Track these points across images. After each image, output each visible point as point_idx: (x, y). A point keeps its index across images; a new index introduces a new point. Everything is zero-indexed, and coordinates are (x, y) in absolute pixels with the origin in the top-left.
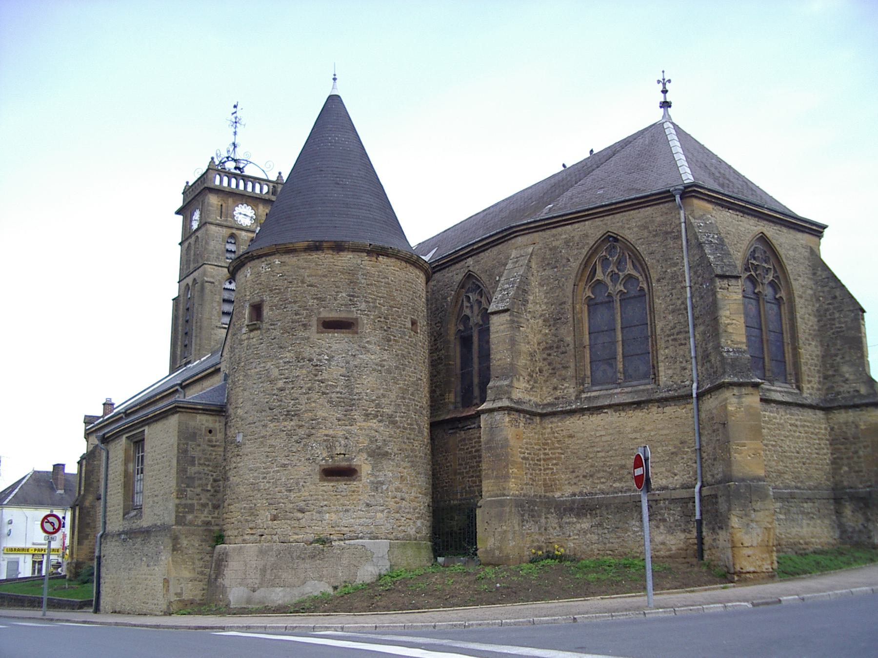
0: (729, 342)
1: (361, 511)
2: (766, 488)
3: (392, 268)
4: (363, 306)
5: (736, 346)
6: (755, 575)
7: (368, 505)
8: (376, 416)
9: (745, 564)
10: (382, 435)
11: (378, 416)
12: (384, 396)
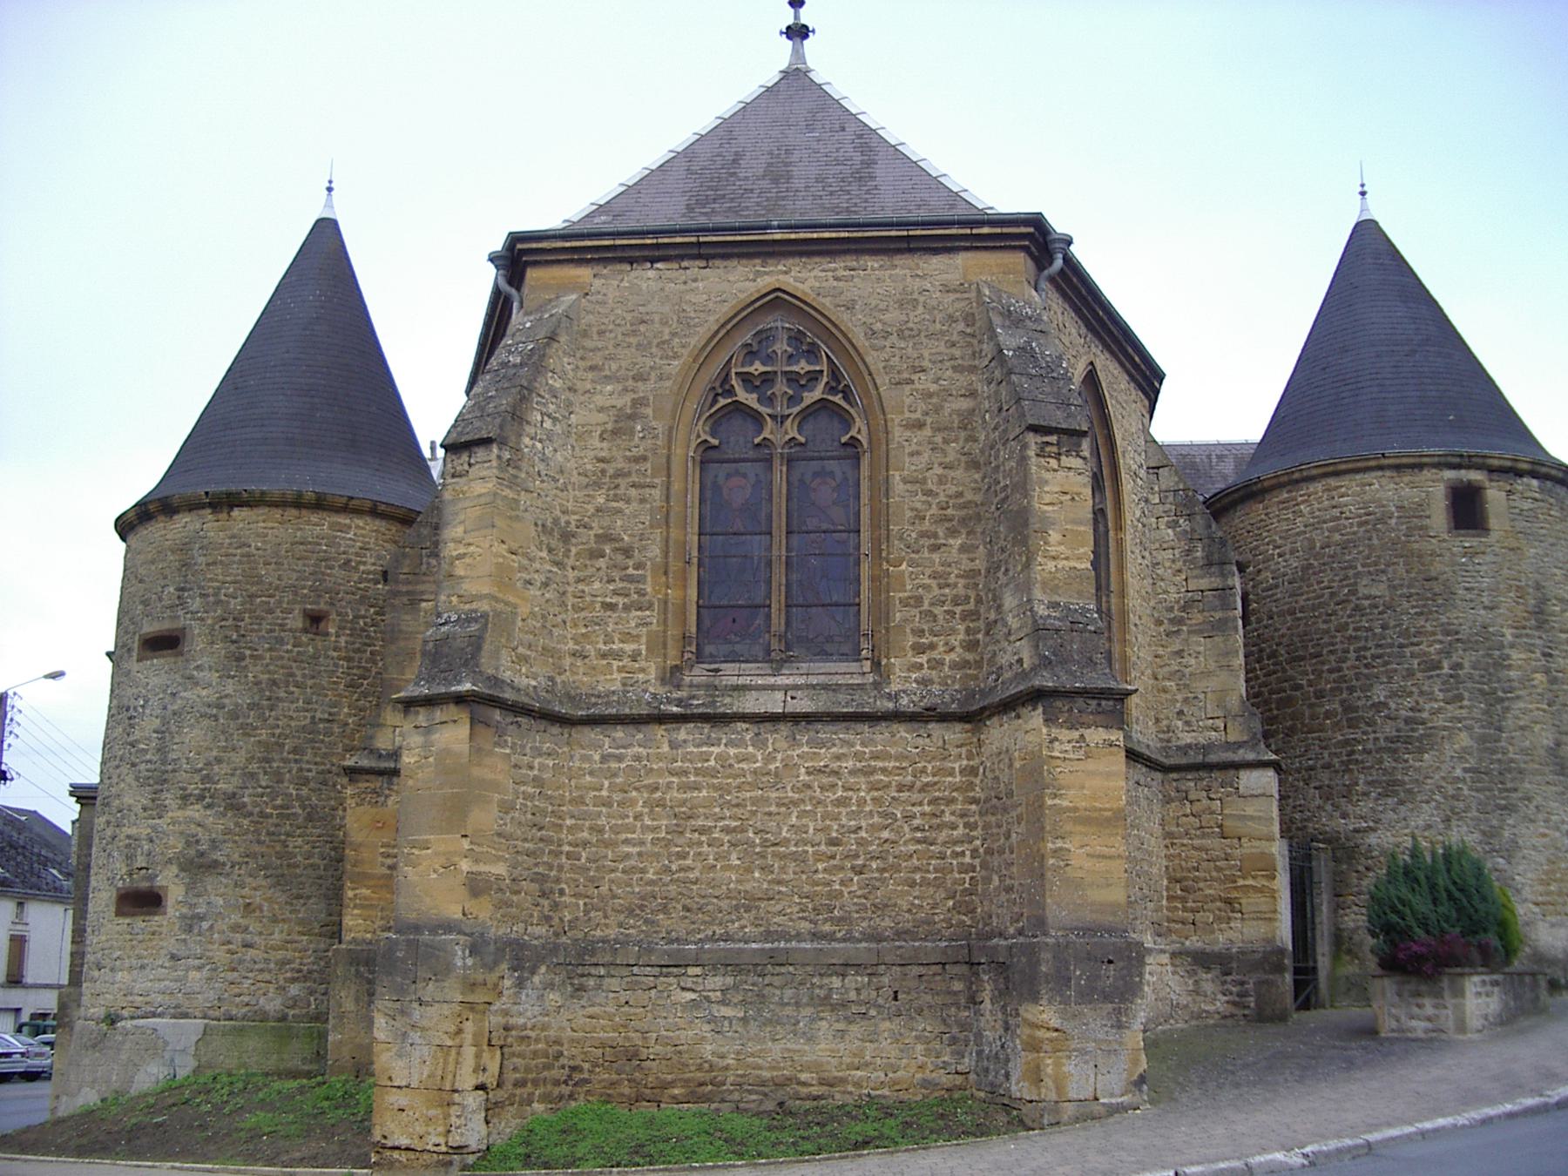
0: (454, 599)
1: (162, 967)
2: (449, 949)
3: (262, 525)
4: (196, 604)
5: (467, 607)
6: (411, 1155)
7: (173, 957)
8: (201, 798)
9: (392, 1126)
10: (209, 831)
11: (205, 797)
12: (219, 761)
